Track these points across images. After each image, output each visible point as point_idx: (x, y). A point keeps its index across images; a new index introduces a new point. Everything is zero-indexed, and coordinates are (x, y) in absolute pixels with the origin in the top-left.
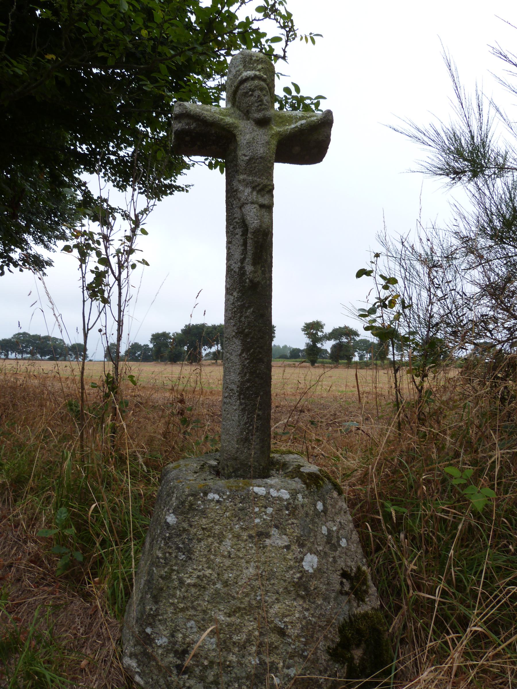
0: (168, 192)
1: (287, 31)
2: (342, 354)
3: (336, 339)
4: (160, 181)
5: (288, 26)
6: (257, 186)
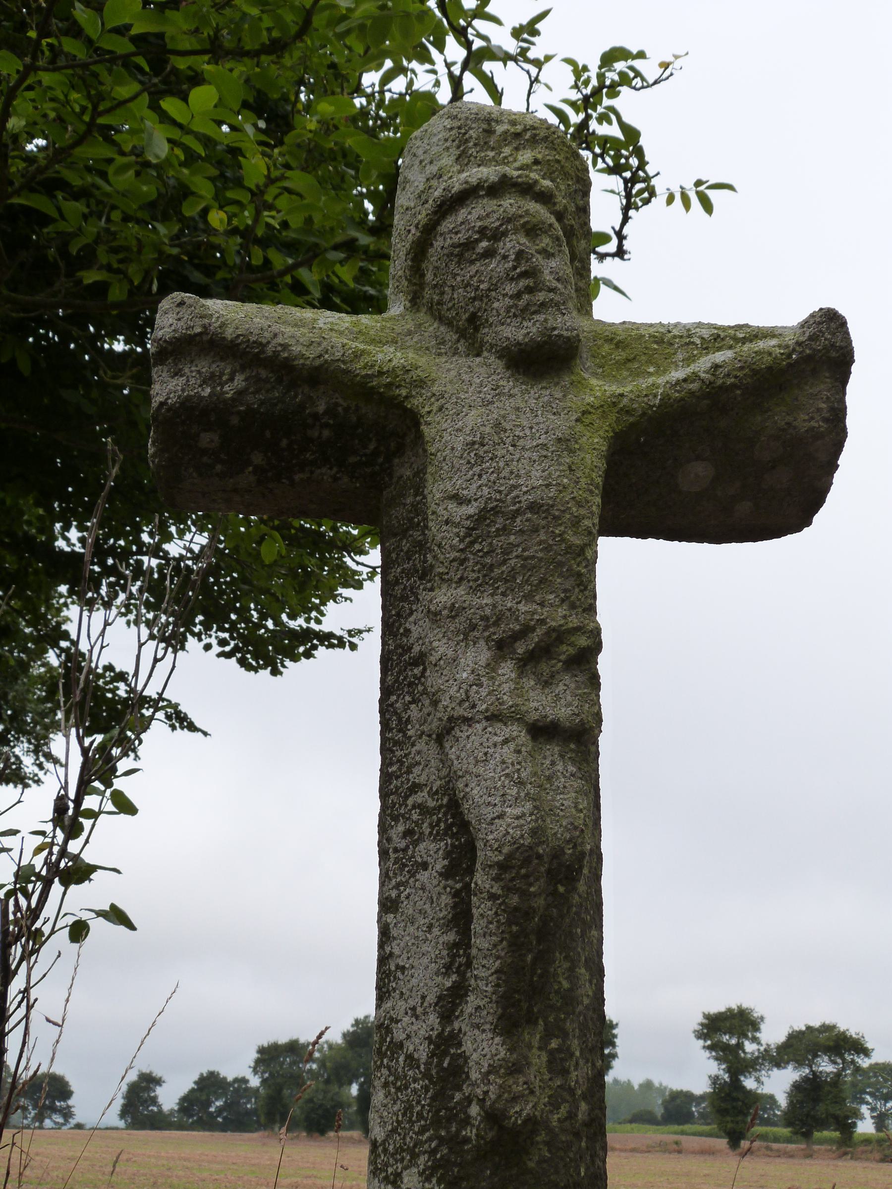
0: (301, 649)
1: (626, 181)
2: (821, 1108)
3: (800, 1063)
4: (278, 622)
5: (627, 167)
6: (516, 636)
